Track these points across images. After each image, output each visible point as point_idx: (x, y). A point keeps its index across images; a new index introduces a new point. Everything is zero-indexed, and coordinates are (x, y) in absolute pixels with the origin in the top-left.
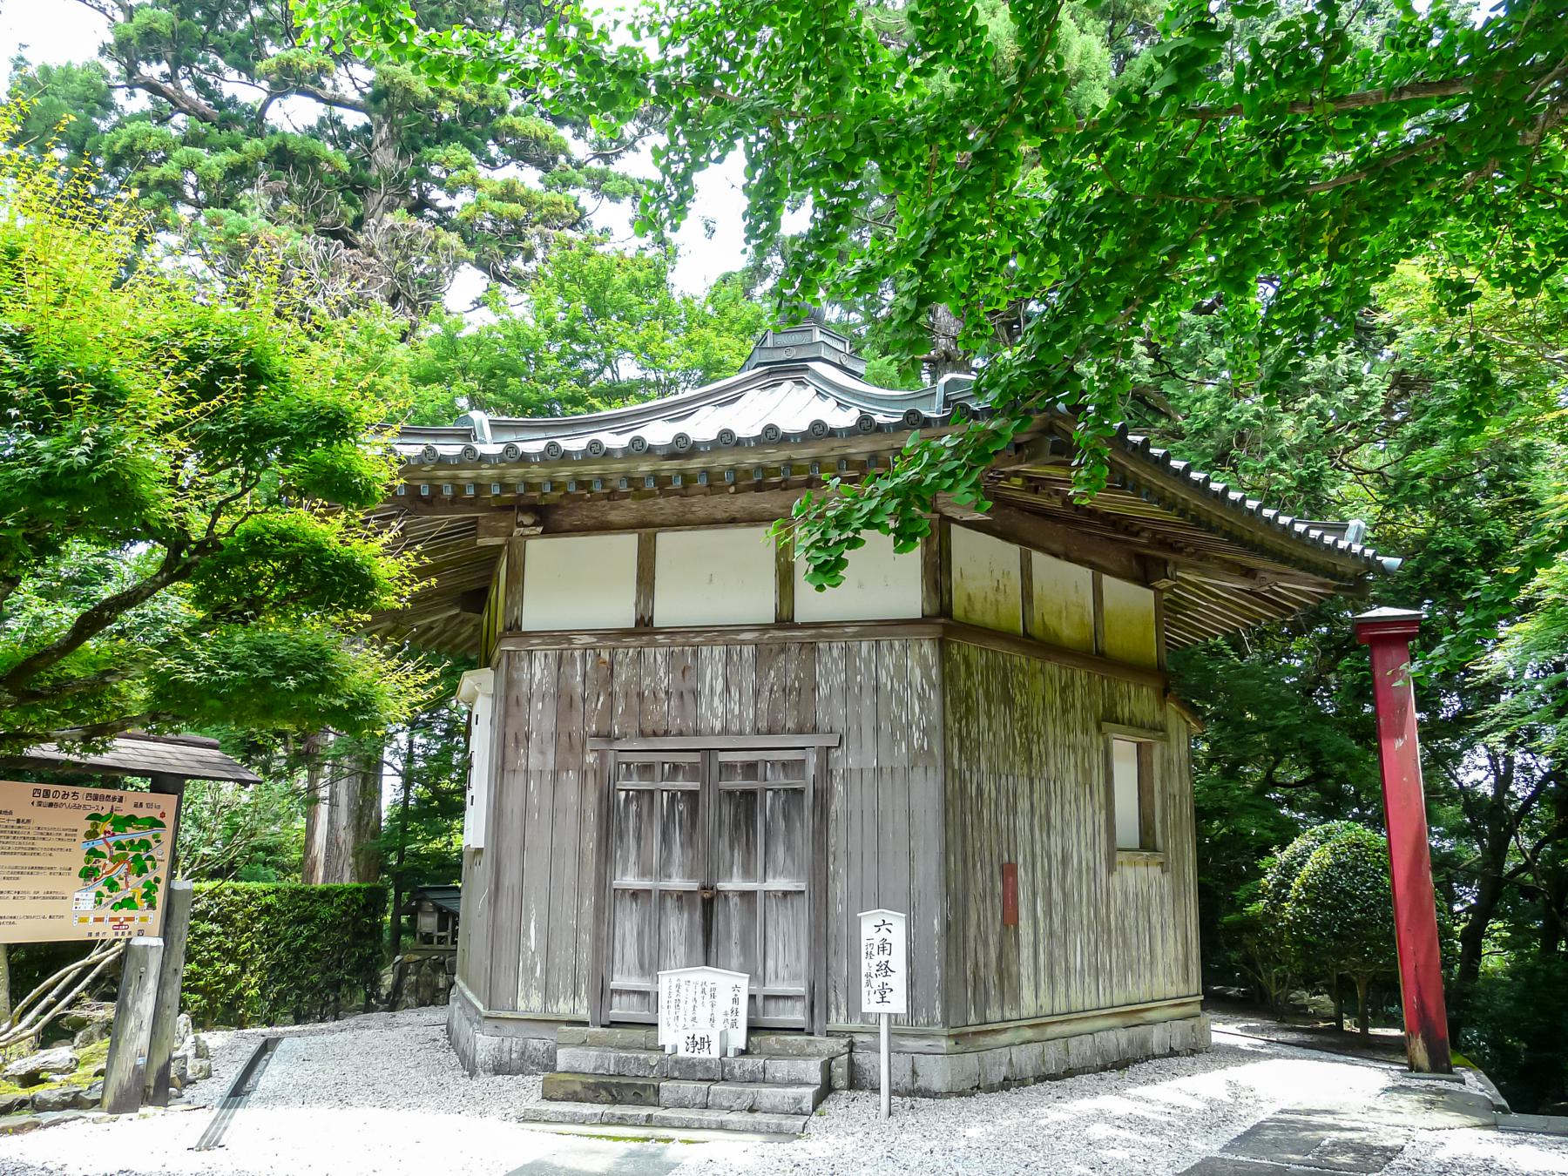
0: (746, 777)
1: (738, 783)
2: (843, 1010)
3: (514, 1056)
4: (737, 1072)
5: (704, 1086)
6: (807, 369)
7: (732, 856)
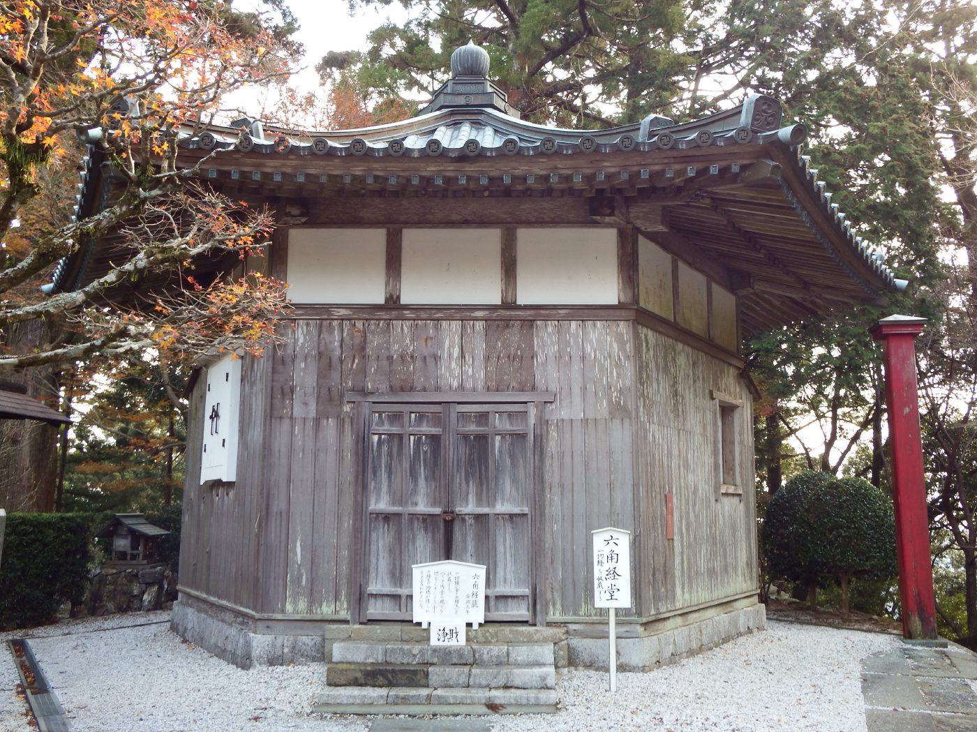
0: (479, 424)
1: (472, 428)
2: (559, 606)
3: (286, 650)
4: (485, 657)
5: (466, 669)
6: (482, 113)
7: (468, 486)
